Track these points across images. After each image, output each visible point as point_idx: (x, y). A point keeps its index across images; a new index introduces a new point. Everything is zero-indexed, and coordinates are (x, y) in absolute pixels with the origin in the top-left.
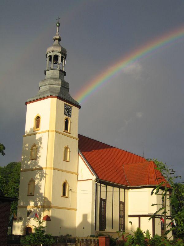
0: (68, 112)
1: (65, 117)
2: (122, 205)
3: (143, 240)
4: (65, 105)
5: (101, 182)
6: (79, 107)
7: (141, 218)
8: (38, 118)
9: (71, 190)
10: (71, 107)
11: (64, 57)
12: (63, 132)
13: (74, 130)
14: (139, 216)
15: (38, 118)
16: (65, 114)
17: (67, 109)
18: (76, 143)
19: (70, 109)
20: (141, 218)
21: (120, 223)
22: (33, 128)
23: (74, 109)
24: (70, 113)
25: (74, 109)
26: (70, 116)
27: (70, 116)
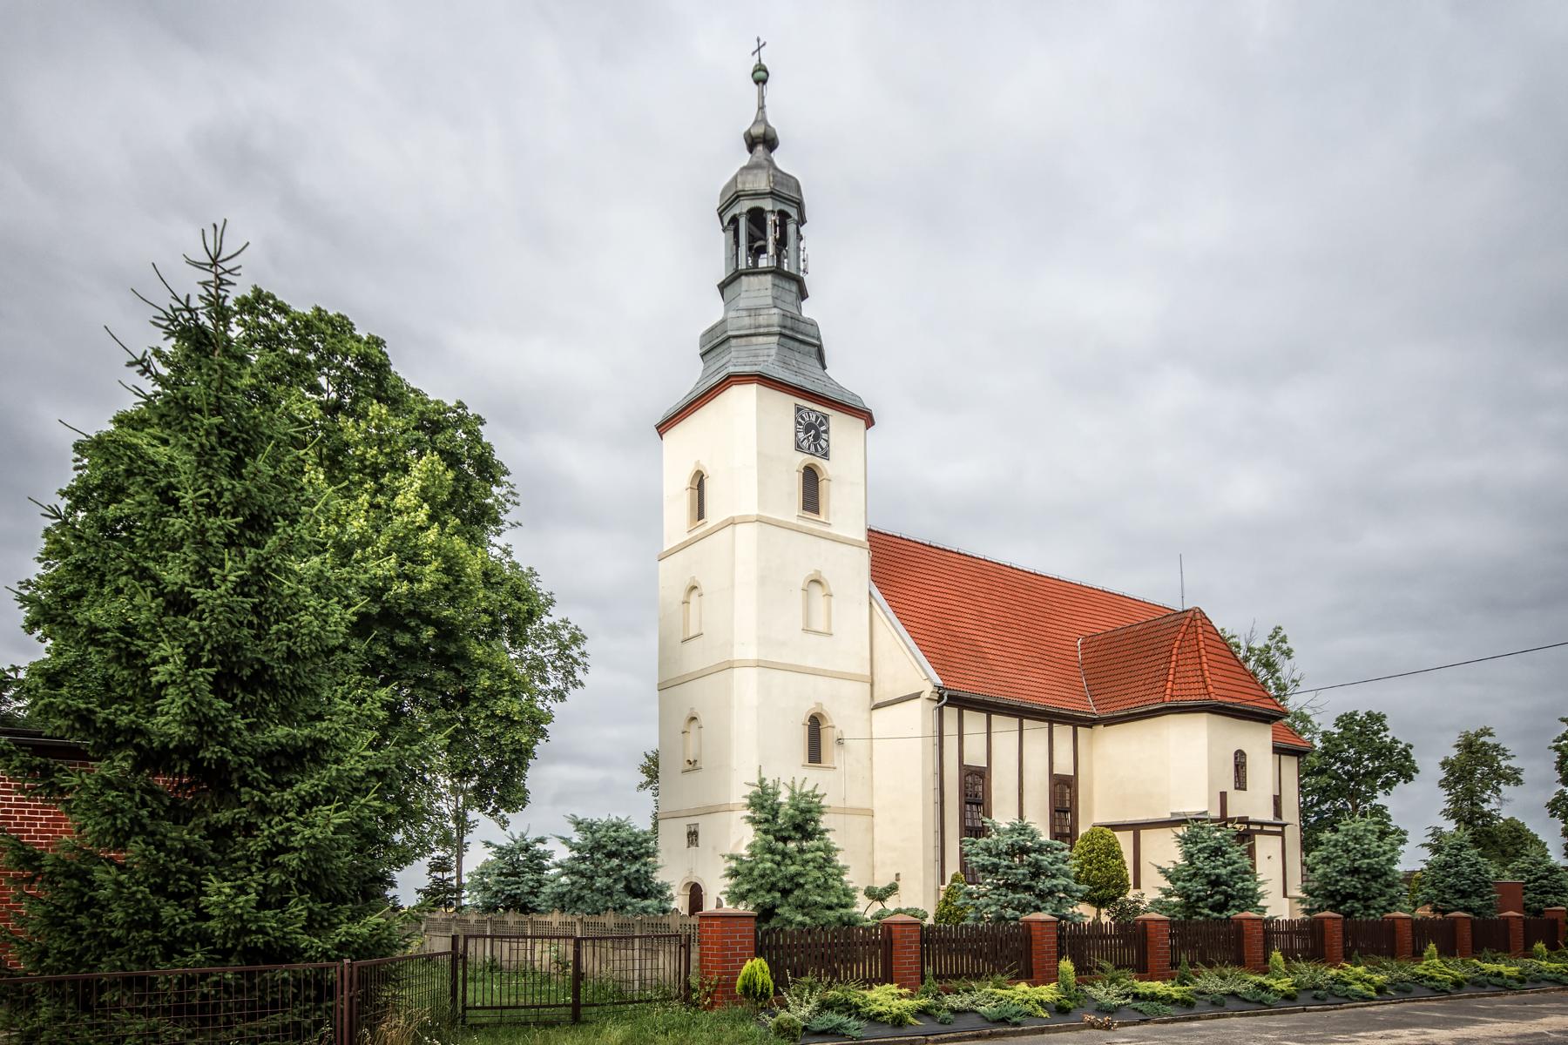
0: (813, 435)
1: (803, 459)
2: (1064, 793)
3: (161, 802)
4: (799, 409)
5: (962, 703)
6: (868, 418)
7: (1142, 832)
8: (699, 482)
9: (840, 741)
10: (826, 417)
11: (793, 212)
12: (794, 520)
13: (847, 513)
14: (1136, 828)
15: (699, 482)
16: (798, 447)
17: (809, 427)
18: (861, 560)
19: (821, 424)
20: (1142, 832)
21: (969, 823)
22: (1263, 910)
23: (841, 429)
24: (823, 444)
25: (841, 429)
26: (826, 456)
27: (826, 456)
